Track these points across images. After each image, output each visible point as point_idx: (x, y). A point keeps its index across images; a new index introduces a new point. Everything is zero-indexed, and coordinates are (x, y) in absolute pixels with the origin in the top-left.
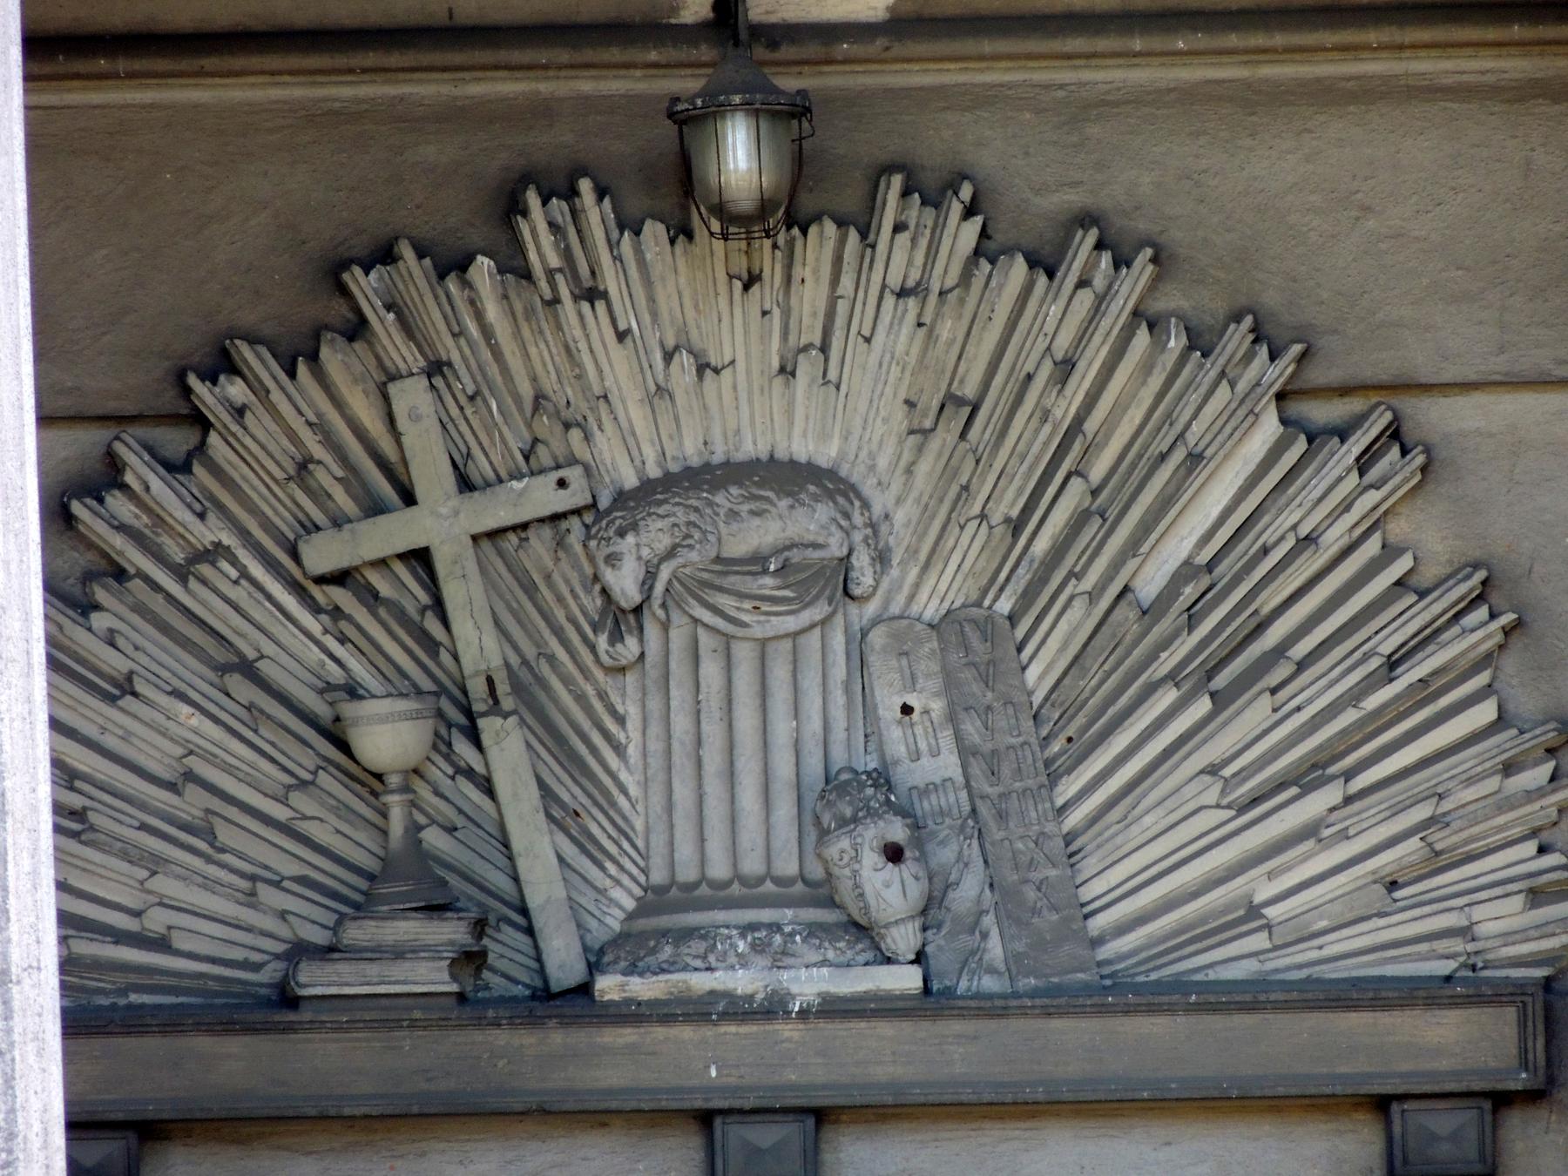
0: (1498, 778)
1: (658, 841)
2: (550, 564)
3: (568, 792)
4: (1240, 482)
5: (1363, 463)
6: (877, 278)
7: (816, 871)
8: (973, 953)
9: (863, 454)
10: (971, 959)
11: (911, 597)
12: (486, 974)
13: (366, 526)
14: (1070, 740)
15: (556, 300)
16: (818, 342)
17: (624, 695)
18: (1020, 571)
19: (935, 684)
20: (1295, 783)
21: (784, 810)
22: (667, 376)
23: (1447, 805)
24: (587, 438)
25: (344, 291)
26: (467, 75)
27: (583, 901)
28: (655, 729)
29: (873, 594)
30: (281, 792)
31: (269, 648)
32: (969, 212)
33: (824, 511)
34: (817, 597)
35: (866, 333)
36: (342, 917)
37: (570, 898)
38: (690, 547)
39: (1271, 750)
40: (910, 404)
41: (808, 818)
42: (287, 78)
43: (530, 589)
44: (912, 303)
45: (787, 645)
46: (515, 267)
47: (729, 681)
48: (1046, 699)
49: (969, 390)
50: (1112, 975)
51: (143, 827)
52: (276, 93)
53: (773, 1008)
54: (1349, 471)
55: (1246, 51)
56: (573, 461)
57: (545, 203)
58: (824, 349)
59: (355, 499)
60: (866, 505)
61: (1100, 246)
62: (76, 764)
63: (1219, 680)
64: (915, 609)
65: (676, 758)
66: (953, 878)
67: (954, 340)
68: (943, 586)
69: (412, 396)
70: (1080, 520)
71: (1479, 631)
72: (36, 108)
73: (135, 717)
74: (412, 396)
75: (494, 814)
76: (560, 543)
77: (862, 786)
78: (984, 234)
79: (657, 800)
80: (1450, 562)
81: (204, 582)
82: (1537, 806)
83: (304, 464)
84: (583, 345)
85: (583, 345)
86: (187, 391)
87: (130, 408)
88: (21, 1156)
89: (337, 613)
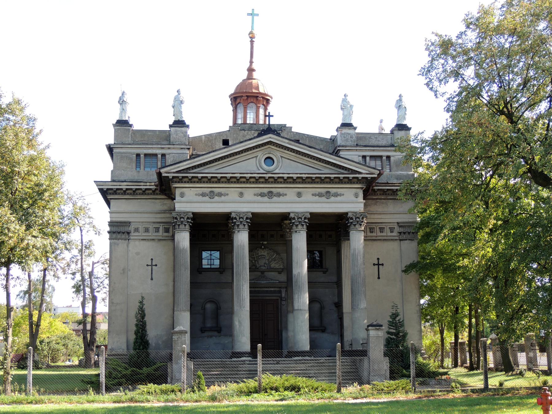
63: (275, 261)
72: (114, 233)
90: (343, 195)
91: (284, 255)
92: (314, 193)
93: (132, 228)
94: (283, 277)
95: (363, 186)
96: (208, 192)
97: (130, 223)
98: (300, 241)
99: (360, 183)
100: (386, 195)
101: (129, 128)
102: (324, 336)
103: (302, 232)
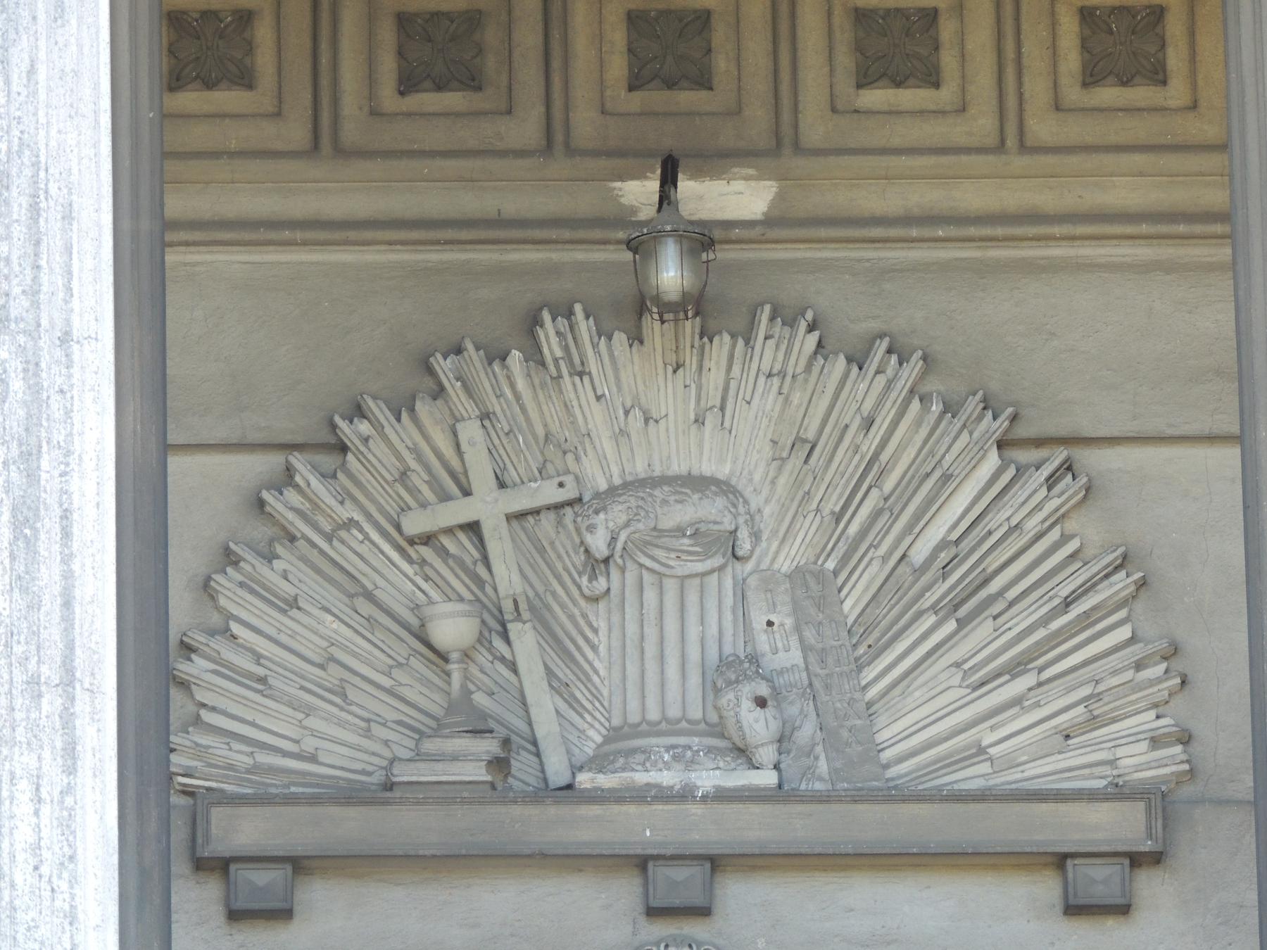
0: (1131, 672)
1: (617, 700)
2: (554, 536)
3: (563, 672)
4: (974, 493)
5: (1051, 482)
6: (754, 366)
7: (713, 717)
8: (809, 768)
9: (745, 472)
10: (809, 772)
11: (774, 559)
12: (510, 780)
13: (441, 507)
14: (870, 646)
15: (560, 376)
16: (718, 405)
17: (597, 616)
18: (840, 544)
19: (787, 609)
20: (1008, 673)
21: (694, 679)
22: (626, 424)
23: (1101, 688)
24: (577, 459)
25: (431, 371)
26: (508, 247)
27: (570, 737)
28: (616, 633)
29: (750, 557)
30: (386, 669)
31: (381, 582)
32: (811, 328)
33: (720, 502)
34: (715, 553)
35: (748, 398)
36: (418, 741)
37: (563, 736)
38: (639, 521)
39: (993, 653)
40: (774, 442)
41: (709, 685)
42: (398, 247)
43: (542, 551)
44: (776, 381)
45: (697, 581)
46: (535, 355)
47: (661, 601)
48: (856, 621)
49: (810, 435)
50: (895, 787)
51: (302, 688)
52: (393, 257)
53: (685, 795)
54: (1041, 486)
55: (982, 239)
56: (568, 472)
57: (554, 320)
58: (722, 409)
59: (435, 493)
60: (746, 502)
61: (889, 351)
62: (262, 651)
63: (964, 607)
64: (776, 566)
65: (628, 650)
66: (797, 724)
67: (801, 405)
68: (793, 553)
69: (471, 431)
70: (876, 514)
71: (1121, 583)
73: (299, 622)
74: (471, 431)
75: (517, 684)
76: (560, 523)
77: (741, 662)
78: (820, 345)
79: (616, 675)
80: (1102, 546)
81: (343, 542)
82: (1155, 689)
83: (404, 475)
84: (575, 403)
85: (575, 403)
86: (334, 427)
87: (300, 439)
88: (76, 468)
89: (424, 562)
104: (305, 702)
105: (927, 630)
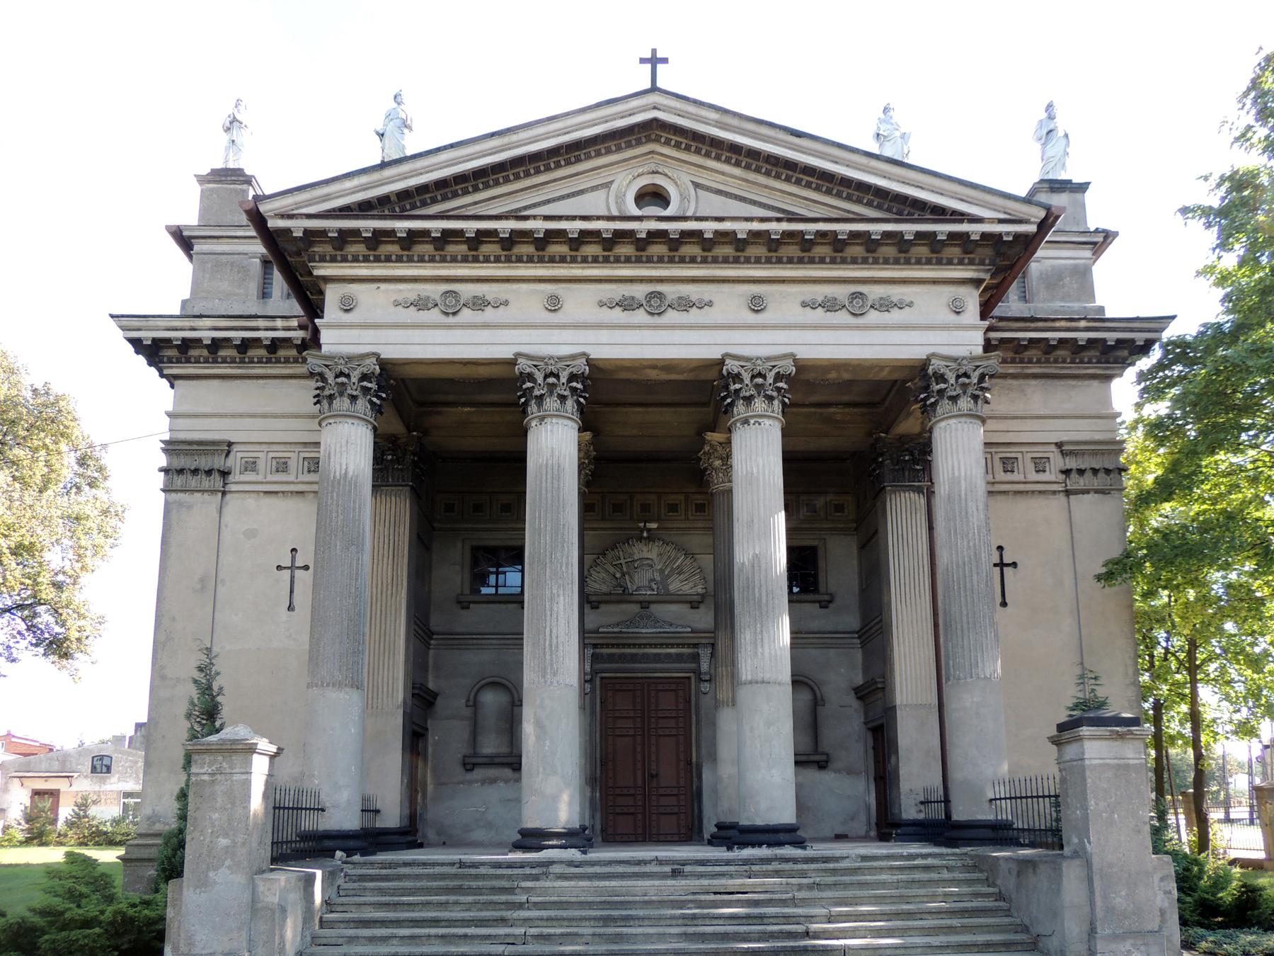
63: (680, 573)
72: (180, 471)
90: (910, 305)
91: (707, 561)
92: (807, 298)
93: (234, 461)
94: (703, 618)
95: (982, 275)
96: (437, 298)
97: (230, 444)
98: (756, 457)
99: (971, 263)
100: (1022, 361)
101: (245, 187)
102: (826, 777)
103: (767, 422)
104: (600, 584)
105: (675, 576)
